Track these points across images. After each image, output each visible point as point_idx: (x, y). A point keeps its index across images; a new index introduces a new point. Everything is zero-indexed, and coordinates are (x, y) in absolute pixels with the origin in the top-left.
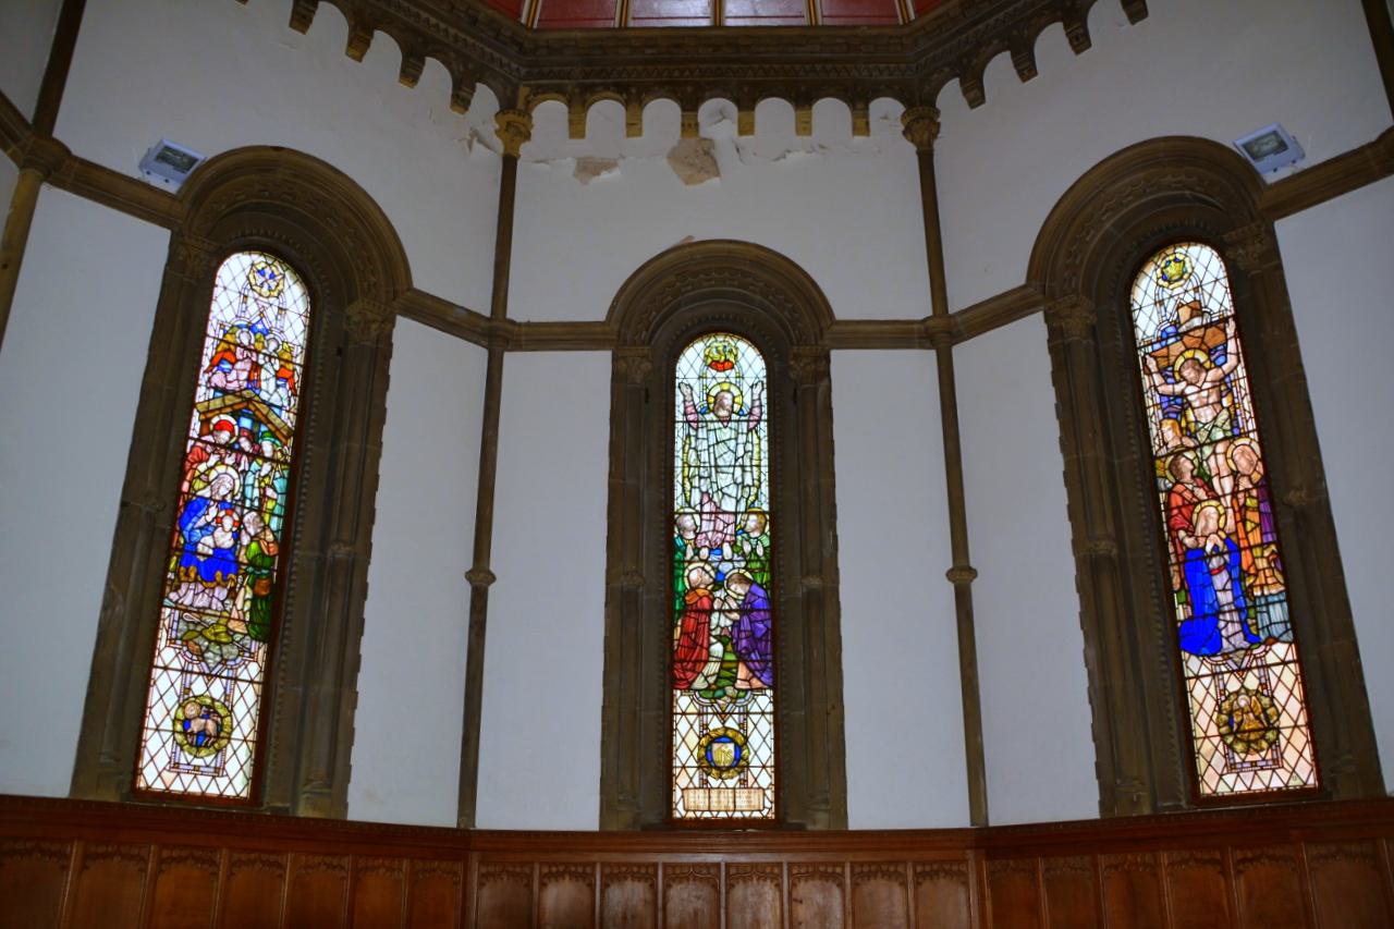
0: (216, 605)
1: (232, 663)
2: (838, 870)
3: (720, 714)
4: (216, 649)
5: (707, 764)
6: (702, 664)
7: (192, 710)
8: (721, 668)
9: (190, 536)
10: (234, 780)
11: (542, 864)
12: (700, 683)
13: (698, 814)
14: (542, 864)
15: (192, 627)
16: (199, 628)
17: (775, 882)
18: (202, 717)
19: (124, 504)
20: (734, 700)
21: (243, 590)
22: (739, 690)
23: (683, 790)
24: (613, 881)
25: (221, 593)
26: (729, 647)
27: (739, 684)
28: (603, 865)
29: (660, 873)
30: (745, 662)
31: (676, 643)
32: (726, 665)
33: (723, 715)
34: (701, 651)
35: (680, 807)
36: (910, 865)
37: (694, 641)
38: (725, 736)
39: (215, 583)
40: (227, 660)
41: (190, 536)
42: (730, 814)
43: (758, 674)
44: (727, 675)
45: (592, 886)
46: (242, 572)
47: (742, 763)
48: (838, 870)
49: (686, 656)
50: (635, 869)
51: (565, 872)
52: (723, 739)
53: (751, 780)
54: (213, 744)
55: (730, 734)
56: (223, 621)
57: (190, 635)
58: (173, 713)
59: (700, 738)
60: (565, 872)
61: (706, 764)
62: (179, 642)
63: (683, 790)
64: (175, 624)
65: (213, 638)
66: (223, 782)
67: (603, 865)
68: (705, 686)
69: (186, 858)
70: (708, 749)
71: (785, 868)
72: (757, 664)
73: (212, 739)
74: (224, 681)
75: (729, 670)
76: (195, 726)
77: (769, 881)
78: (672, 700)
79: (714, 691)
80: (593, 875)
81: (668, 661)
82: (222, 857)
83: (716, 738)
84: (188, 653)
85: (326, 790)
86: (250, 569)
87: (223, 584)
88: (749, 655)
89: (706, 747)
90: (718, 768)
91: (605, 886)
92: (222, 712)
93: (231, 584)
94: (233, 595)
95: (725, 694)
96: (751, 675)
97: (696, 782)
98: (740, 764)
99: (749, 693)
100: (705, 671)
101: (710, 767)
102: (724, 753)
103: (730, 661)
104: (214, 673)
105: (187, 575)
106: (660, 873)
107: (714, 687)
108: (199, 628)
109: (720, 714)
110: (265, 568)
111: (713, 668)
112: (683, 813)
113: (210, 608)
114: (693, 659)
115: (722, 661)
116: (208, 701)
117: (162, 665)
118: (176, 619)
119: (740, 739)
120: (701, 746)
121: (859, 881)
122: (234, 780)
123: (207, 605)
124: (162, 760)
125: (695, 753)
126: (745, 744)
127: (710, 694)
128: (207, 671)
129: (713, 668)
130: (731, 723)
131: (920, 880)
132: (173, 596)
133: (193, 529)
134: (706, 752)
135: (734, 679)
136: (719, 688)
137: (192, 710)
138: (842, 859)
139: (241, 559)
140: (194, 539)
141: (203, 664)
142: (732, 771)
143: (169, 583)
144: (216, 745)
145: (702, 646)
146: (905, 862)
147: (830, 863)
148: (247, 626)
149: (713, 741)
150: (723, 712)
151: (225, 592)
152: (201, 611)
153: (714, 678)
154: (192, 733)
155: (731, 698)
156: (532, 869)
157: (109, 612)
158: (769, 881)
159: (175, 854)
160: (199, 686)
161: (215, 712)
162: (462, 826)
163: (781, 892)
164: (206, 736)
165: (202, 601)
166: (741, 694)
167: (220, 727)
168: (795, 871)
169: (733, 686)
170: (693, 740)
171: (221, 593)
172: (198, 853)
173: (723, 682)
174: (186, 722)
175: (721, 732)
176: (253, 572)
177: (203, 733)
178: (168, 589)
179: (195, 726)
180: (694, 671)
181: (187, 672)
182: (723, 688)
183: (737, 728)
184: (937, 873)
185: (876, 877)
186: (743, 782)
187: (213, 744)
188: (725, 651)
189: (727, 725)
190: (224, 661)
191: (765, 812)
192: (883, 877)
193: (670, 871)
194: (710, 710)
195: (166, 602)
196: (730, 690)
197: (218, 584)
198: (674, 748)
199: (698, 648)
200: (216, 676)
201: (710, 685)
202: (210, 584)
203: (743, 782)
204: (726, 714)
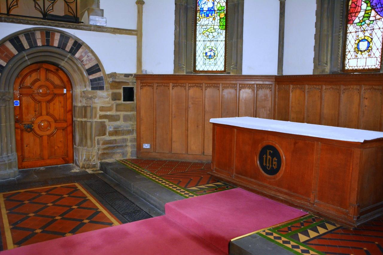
0: (210, 23)
1: (216, 37)
2: (218, 85)
3: (363, 31)
4: (211, 34)
5: (358, 50)
6: (358, 13)
7: (207, 50)
8: (365, 13)
9: (201, 7)
10: (220, 67)
11: (205, 84)
12: (357, 20)
13: (353, 68)
14: (189, 83)
15: (204, 29)
16: (206, 29)
17: (270, 89)
18: (210, 51)
19: (176, 4)
20: (368, 25)
21: (217, 17)
22: (371, 21)
23: (349, 59)
24: (242, 89)
25: (211, 19)
26: (369, 5)
27: (371, 19)
28: (240, 84)
29: (238, 86)
30: (374, 9)
31: (349, 7)
32: (367, 12)
33: (364, 31)
34: (358, 8)
35: (347, 66)
36: (221, 84)
37: (356, 5)
38: (364, 39)
39: (209, 17)
40: (214, 36)
41: (201, 7)
42: (364, 67)
43: (379, 13)
44: (367, 15)
45: (236, 90)
46: (216, 12)
47: (370, 48)
48: (218, 85)
49: (352, 11)
50: (248, 85)
51: (195, 86)
52: (363, 40)
53: (372, 54)
54: (213, 58)
55: (366, 38)
56: (212, 27)
57: (204, 32)
58: (202, 52)
59: (355, 41)
60: (195, 86)
61: (357, 50)
62: (202, 34)
63: (349, 59)
64: (200, 30)
65: (210, 31)
66: (217, 67)
67: (240, 84)
68: (359, 21)
69: (178, 85)
70: (358, 44)
71: (238, 84)
72: (379, 9)
73: (213, 57)
74: (214, 42)
75: (368, 14)
76: (209, 54)
77: (268, 89)
78: (347, 27)
79: (361, 23)
80: (237, 87)
81: (345, 14)
82: (155, 85)
83: (361, 40)
84: (204, 36)
85: (235, 67)
86: (218, 11)
87: (211, 17)
88: (376, 6)
89: (357, 44)
90: (361, 51)
91: (257, 90)
92: (215, 50)
93: (213, 16)
94: (214, 19)
95: (365, 23)
96: (376, 14)
97: (353, 57)
98: (369, 49)
99: (375, 21)
100: (359, 16)
101: (358, 51)
102: (363, 46)
103: (369, 10)
104: (211, 40)
105: (202, 17)
106: (238, 86)
107: (361, 21)
108: (206, 29)
109: (363, 31)
110: (222, 10)
111: (362, 14)
112: (348, 67)
113: (209, 24)
114: (355, 12)
115: (366, 10)
116: (211, 48)
117: (349, 32)
118: (200, 28)
119: (369, 40)
120: (356, 44)
121: (224, 89)
122: (220, 67)
123: (208, 23)
124: (201, 63)
125: (353, 47)
126: (371, 41)
127: (360, 24)
128: (210, 40)
129: (362, 14)
130: (367, 34)
131: (258, 89)
132: (199, 23)
133: (202, 4)
134: (357, 46)
135: (369, 17)
136: (363, 21)
137: (207, 50)
138: (219, 83)
139: (215, 10)
140: (202, 7)
141: (208, 38)
142: (366, 52)
143: (198, 20)
144: (214, 58)
145: (359, 6)
146: (186, 83)
147: (199, 83)
148: (219, 27)
149: (360, 41)
150: (364, 30)
151: (212, 19)
152: (206, 25)
153: (362, 18)
154: (208, 56)
155: (368, 24)
156: (220, 85)
157: (176, 31)
158: (268, 89)
159: (192, 85)
160: (208, 44)
161: (213, 50)
162: (316, 74)
163: (254, 92)
164: (211, 56)
165: (206, 22)
166: (372, 22)
167: (215, 54)
168: (258, 86)
169: (369, 20)
170: (353, 42)
171: (211, 19)
172: (148, 84)
173: (365, 19)
174: (206, 53)
175: (363, 38)
176: (219, 12)
177: (210, 56)
178: (197, 21)
179: (209, 54)
180: (355, 16)
181: (357, 32)
182: (365, 21)
183: (369, 36)
184: (194, 86)
185: (246, 88)
186: (369, 55)
187: (213, 58)
188: (367, 6)
189: (365, 35)
190: (214, 37)
191: (376, 66)
192: (230, 88)
193: (241, 86)
194: (360, 30)
195: (198, 25)
196: (367, 22)
197: (210, 17)
198: (347, 45)
199: (357, 7)
200: (212, 41)
201: (360, 20)
202: (208, 18)
203: (369, 55)
204: (365, 31)
